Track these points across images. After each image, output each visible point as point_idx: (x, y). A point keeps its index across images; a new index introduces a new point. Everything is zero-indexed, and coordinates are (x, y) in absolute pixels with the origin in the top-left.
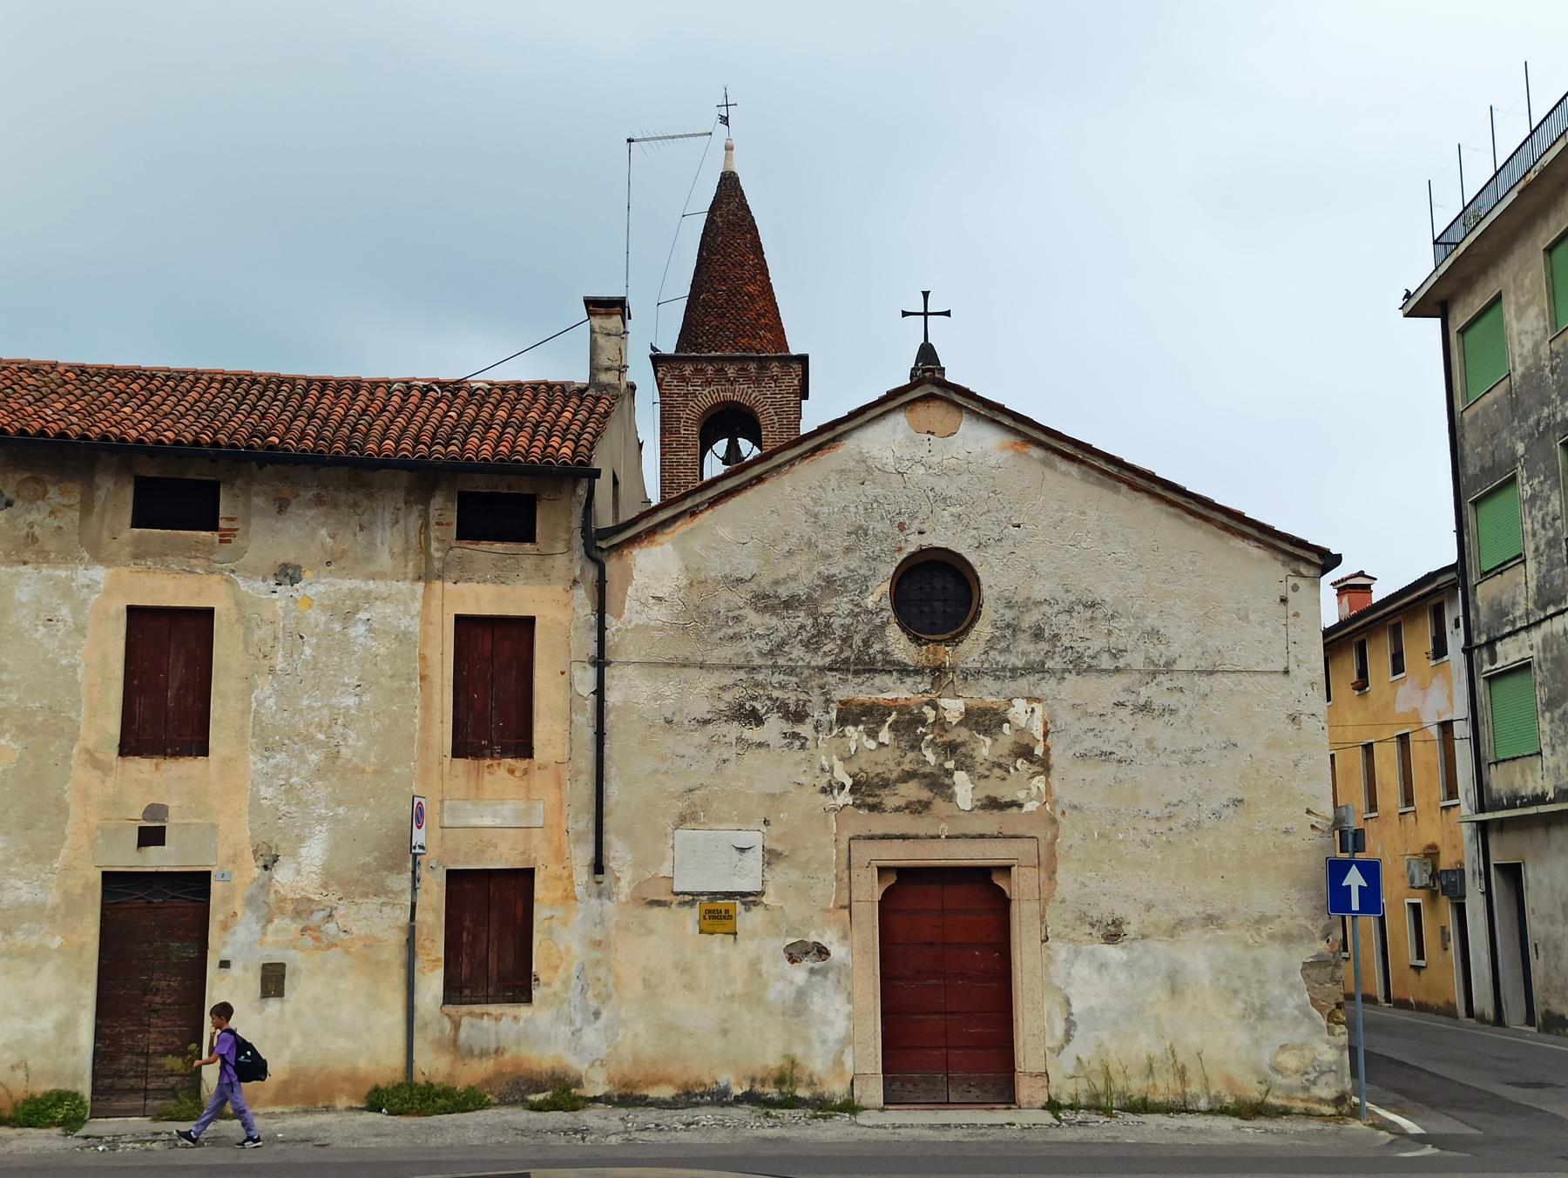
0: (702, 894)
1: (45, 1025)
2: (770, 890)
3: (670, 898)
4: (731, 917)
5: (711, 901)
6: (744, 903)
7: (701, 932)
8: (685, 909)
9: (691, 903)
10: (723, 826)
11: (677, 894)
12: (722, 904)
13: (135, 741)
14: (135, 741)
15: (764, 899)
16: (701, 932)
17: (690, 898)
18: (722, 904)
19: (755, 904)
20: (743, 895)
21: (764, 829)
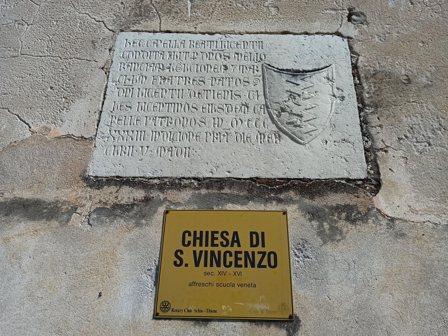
0: (177, 184)
1: (125, 256)
2: (395, 170)
3: (67, 194)
4: (272, 260)
5: (205, 204)
6: (314, 214)
7: (162, 312)
8: (117, 232)
9: (137, 212)
10: (242, 27)
11: (98, 183)
12: (240, 216)
13: (242, 267)
14: (242, 267)
15: (380, 201)
16: (162, 312)
17: (136, 197)
18: (240, 216)
19: (353, 215)
20: (308, 187)
21: (350, 30)
